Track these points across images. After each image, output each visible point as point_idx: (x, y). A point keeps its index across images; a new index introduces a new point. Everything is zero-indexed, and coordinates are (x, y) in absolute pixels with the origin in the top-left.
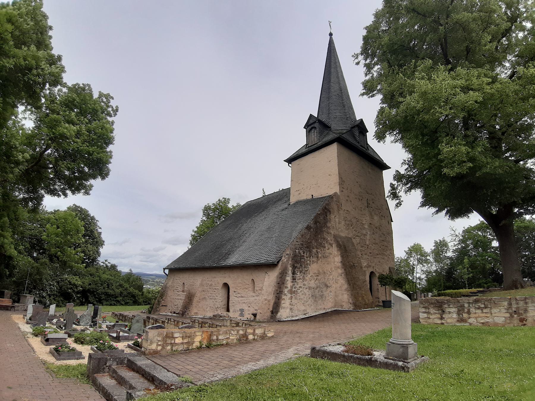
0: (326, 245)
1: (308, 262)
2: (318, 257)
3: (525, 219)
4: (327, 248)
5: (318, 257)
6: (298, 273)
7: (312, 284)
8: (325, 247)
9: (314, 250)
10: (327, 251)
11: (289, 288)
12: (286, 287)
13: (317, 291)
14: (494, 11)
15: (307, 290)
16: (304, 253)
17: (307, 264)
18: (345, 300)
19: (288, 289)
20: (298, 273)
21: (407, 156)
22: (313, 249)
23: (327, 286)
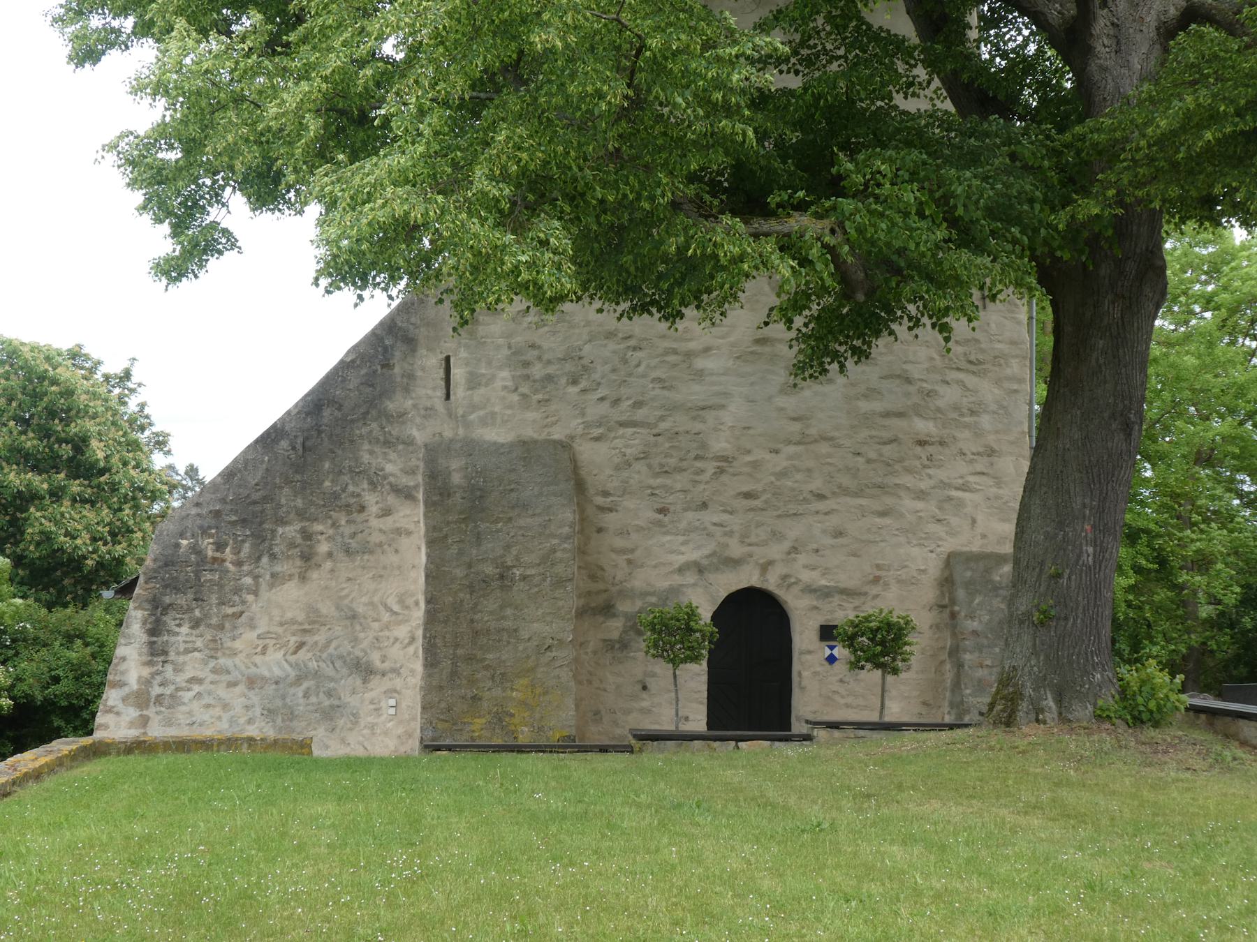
0: (370, 499)
1: (248, 581)
2: (307, 557)
3: (52, 722)
4: (374, 510)
5: (307, 557)
6: (184, 630)
7: (274, 663)
8: (362, 509)
9: (290, 531)
10: (374, 523)
11: (134, 685)
12: (121, 684)
13: (300, 692)
14: (495, 132)
15: (240, 688)
16: (220, 547)
17: (237, 591)
18: (698, 721)
19: (126, 690)
20: (184, 630)
21: (210, 471)
22: (282, 522)
23: (365, 671)
